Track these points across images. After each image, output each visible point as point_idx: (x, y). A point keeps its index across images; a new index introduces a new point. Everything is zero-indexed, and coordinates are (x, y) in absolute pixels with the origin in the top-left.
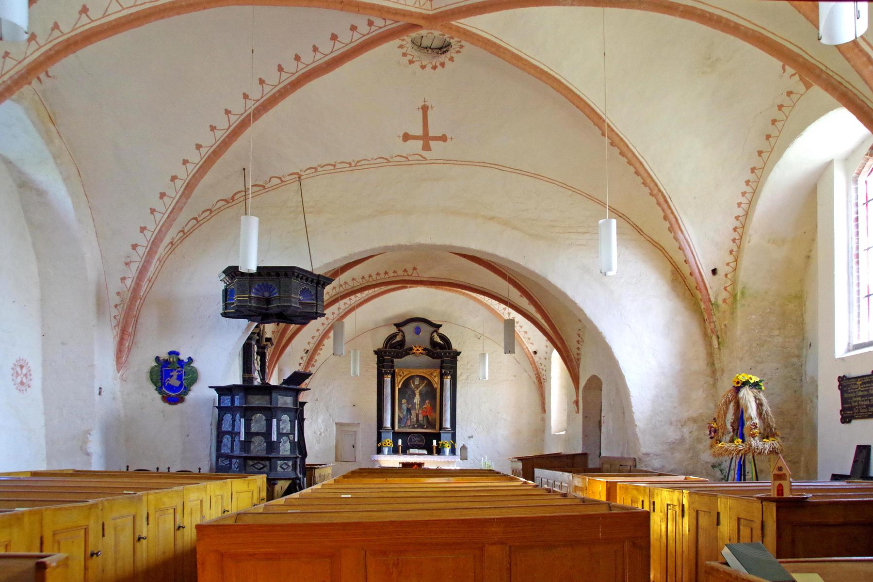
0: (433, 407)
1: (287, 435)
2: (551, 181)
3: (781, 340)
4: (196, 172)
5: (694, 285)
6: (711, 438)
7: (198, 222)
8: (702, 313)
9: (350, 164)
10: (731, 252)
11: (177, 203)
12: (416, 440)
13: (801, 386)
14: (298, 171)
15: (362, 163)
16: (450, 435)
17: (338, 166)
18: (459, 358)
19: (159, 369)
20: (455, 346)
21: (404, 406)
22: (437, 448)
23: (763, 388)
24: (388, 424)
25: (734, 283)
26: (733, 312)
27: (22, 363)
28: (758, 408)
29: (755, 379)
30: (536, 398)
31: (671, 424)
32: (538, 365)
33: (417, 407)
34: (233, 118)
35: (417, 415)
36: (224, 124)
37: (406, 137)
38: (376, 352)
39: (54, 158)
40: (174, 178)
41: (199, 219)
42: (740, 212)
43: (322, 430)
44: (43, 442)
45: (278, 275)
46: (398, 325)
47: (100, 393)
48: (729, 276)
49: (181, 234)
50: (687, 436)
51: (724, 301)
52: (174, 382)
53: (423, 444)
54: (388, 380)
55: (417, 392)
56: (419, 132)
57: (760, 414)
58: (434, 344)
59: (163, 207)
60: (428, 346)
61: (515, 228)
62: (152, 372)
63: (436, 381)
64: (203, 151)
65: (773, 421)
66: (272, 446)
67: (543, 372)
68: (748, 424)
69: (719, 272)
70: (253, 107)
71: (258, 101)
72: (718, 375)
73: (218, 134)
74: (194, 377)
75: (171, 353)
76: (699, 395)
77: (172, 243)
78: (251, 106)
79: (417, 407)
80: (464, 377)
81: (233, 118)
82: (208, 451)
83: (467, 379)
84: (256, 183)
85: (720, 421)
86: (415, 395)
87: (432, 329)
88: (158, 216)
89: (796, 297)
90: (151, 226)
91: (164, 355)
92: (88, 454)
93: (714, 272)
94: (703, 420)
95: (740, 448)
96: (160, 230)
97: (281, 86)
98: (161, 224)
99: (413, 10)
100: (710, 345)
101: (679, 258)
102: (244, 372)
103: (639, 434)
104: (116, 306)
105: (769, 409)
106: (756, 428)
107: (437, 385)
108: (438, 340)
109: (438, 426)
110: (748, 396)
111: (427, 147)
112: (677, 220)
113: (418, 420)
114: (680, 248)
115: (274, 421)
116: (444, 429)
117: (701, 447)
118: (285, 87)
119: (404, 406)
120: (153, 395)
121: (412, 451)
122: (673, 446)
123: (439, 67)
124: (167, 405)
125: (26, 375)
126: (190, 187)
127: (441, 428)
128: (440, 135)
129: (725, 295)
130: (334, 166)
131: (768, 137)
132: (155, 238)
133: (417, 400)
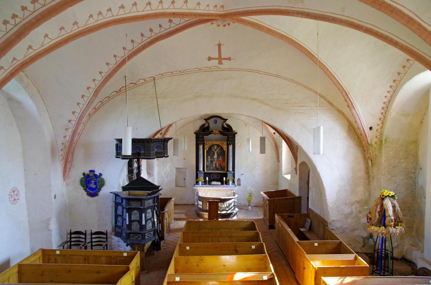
0: (224, 160)
1: (150, 219)
2: (286, 79)
3: (405, 165)
4: (100, 84)
5: (359, 134)
6: (368, 222)
7: (102, 103)
8: (363, 147)
9: (180, 72)
10: (380, 119)
11: (90, 99)
12: (215, 176)
13: (415, 189)
14: (153, 76)
15: (187, 71)
16: (232, 175)
17: (174, 73)
18: (236, 135)
19: (85, 179)
20: (234, 129)
21: (209, 160)
22: (225, 181)
23: (396, 198)
24: (201, 169)
25: (381, 134)
26: (380, 149)
27: (14, 189)
28: (393, 207)
29: (392, 193)
30: (275, 155)
31: (346, 204)
32: (276, 139)
33: (216, 160)
34: (118, 59)
35: (216, 164)
36: (113, 62)
37: (210, 59)
38: (195, 133)
39: (25, 88)
40: (88, 88)
41: (103, 102)
42: (386, 100)
43: (169, 172)
44: (27, 225)
45: (143, 142)
46: (206, 120)
47: (55, 197)
48: (378, 131)
49: (94, 109)
50: (354, 210)
51: (376, 143)
52: (93, 186)
53: (219, 178)
54: (201, 147)
55: (216, 153)
56: (217, 56)
57: (394, 211)
58: (223, 128)
59: (84, 102)
60: (221, 130)
61: (267, 104)
62: (81, 181)
63: (225, 147)
64: (103, 74)
65: (401, 216)
66: (142, 227)
67: (278, 143)
68: (388, 219)
69: (373, 128)
70: (127, 55)
71: (131, 50)
72: (371, 179)
73: (111, 66)
74: (102, 183)
75: (91, 171)
76: (361, 189)
77: (89, 114)
78: (127, 53)
79: (216, 160)
80: (239, 144)
81: (118, 59)
82: (111, 221)
83: (240, 146)
84: (132, 82)
85: (373, 214)
86: (214, 154)
87: (223, 121)
88: (81, 106)
89: (414, 142)
90: (78, 110)
91: (87, 172)
92: (50, 230)
93: (371, 128)
94: (362, 202)
95: (384, 232)
96: (83, 112)
97: (142, 44)
98: (83, 109)
99: (213, 12)
100: (367, 163)
101: (352, 120)
102: (129, 167)
103: (330, 210)
104: (62, 150)
105: (399, 208)
106: (392, 222)
107: (225, 149)
108: (226, 126)
109: (226, 170)
110: (388, 203)
111: (220, 63)
112: (352, 104)
113: (216, 166)
114: (353, 115)
115: (144, 215)
116: (229, 171)
117: (361, 215)
118: (145, 45)
119: (209, 160)
120: (82, 192)
121: (213, 183)
122: (347, 216)
123: (227, 26)
124: (89, 197)
125: (16, 195)
126: (97, 92)
127: (228, 170)
128: (228, 57)
129: (376, 140)
130: (172, 73)
131: (404, 67)
132: (80, 116)
133: (215, 156)
